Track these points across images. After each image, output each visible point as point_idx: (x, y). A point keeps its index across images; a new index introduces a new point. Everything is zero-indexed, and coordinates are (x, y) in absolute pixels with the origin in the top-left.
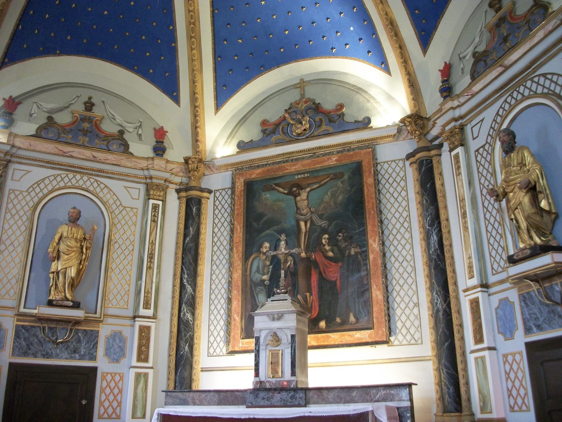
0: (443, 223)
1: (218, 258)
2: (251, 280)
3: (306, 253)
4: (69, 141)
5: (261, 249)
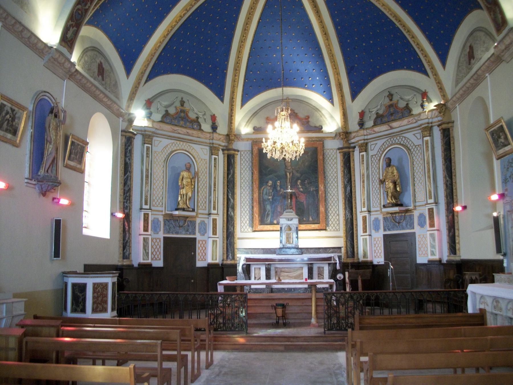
0: (353, 182)
1: (244, 186)
4: (176, 124)
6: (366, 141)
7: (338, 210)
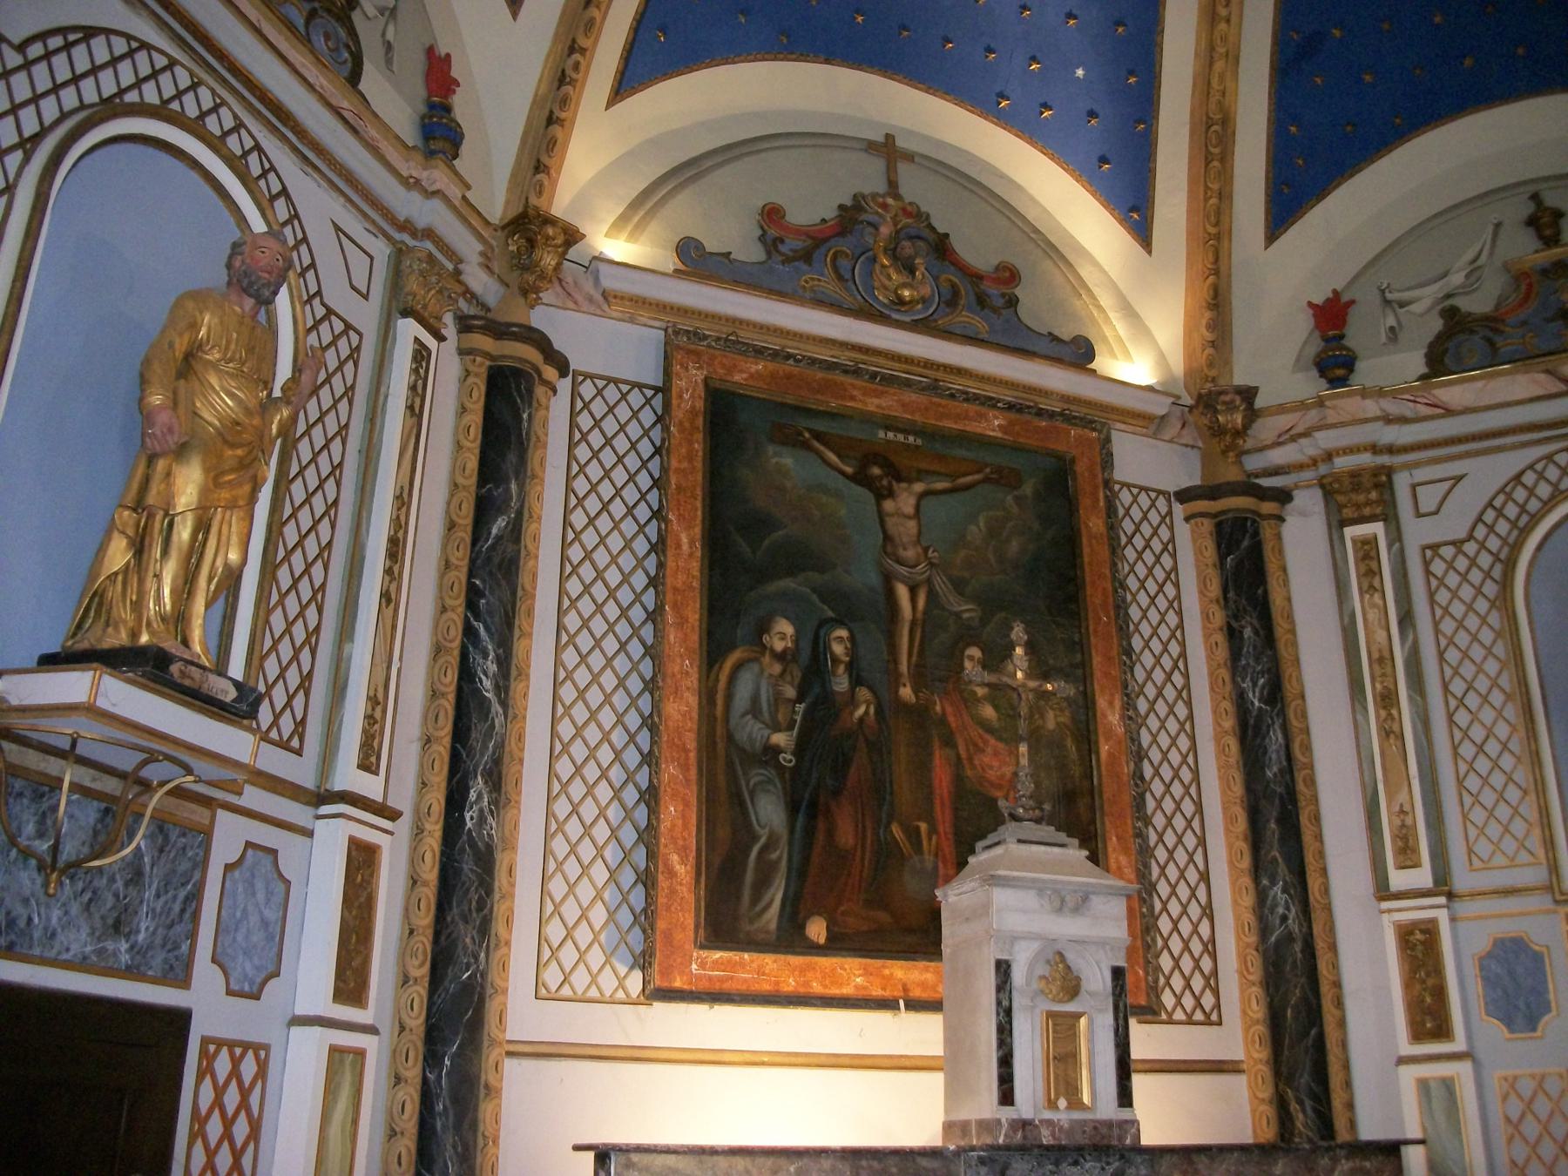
2: (730, 738)
3: (916, 691)
5: (766, 638)
6: (1385, 460)
7: (1205, 877)
